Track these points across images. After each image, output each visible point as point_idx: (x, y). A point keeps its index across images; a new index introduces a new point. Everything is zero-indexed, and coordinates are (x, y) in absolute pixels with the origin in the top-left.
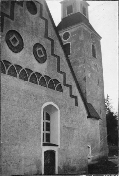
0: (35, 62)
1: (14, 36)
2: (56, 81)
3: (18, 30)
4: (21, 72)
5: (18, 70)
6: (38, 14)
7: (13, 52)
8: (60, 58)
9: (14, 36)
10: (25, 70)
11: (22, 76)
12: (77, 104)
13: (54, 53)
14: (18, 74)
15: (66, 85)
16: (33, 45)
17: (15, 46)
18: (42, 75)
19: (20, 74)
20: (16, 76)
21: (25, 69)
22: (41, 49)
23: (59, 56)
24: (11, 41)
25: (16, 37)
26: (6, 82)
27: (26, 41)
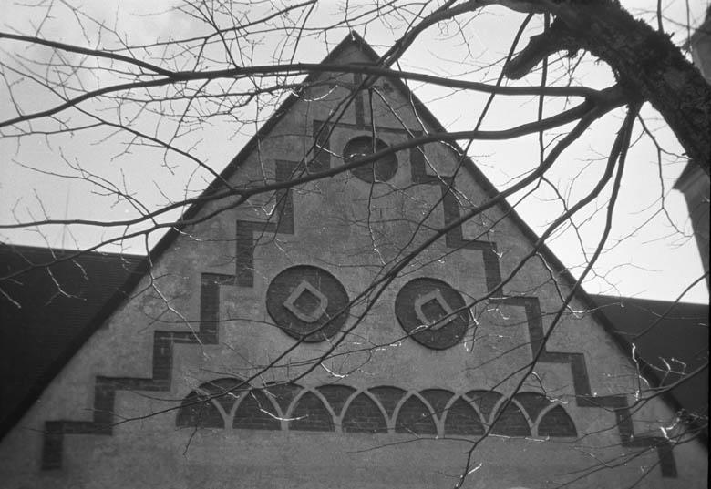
0: (413, 352)
1: (305, 284)
2: (535, 401)
3: (317, 259)
4: (352, 404)
5: (337, 403)
6: (403, 174)
7: (448, 389)
8: (541, 301)
9: (305, 284)
10: (368, 393)
11: (361, 420)
12: (5, 25)
13: (480, 253)
14: (338, 414)
15: (585, 401)
16: (397, 292)
17: (311, 321)
18: (453, 394)
19: (346, 415)
20: (433, 430)
21: (369, 390)
22: (437, 294)
23: (579, 408)
24: (291, 308)
25: (310, 287)
26: (285, 458)
27: (327, 256)
